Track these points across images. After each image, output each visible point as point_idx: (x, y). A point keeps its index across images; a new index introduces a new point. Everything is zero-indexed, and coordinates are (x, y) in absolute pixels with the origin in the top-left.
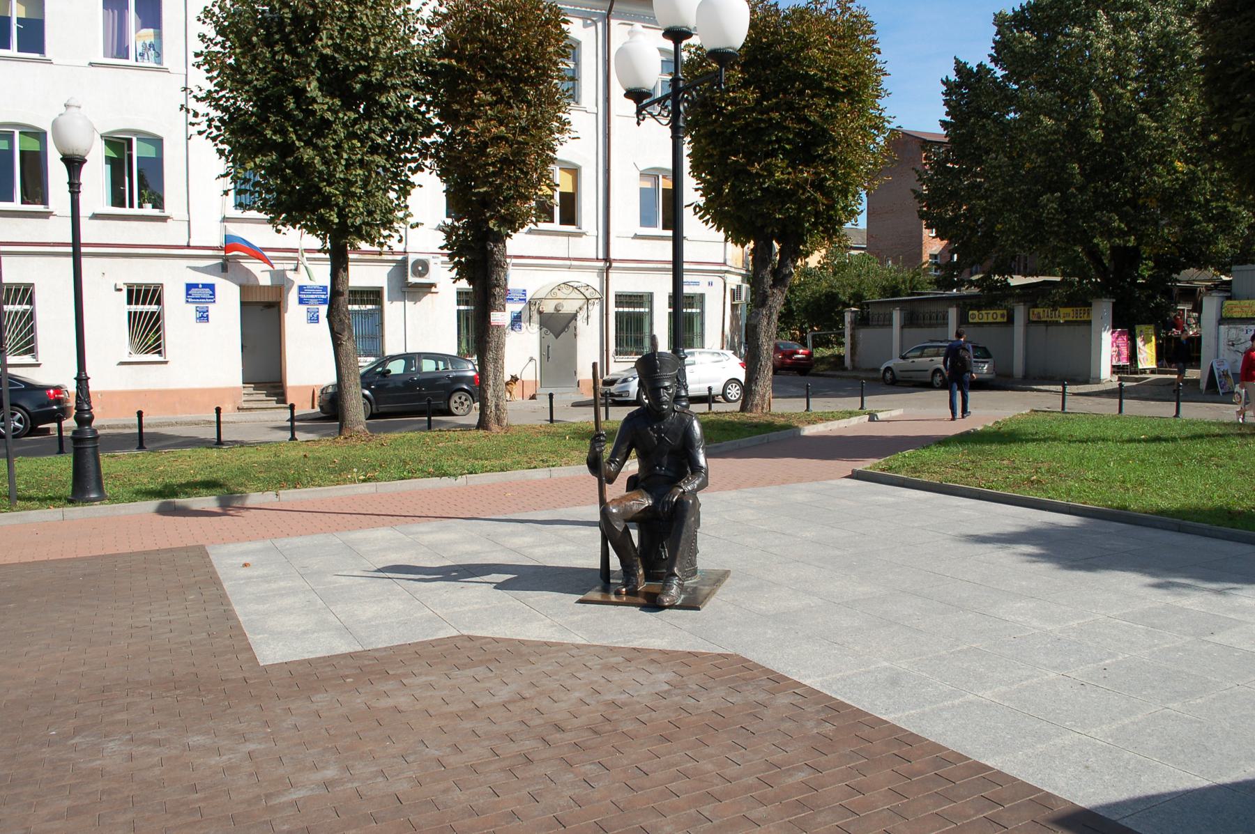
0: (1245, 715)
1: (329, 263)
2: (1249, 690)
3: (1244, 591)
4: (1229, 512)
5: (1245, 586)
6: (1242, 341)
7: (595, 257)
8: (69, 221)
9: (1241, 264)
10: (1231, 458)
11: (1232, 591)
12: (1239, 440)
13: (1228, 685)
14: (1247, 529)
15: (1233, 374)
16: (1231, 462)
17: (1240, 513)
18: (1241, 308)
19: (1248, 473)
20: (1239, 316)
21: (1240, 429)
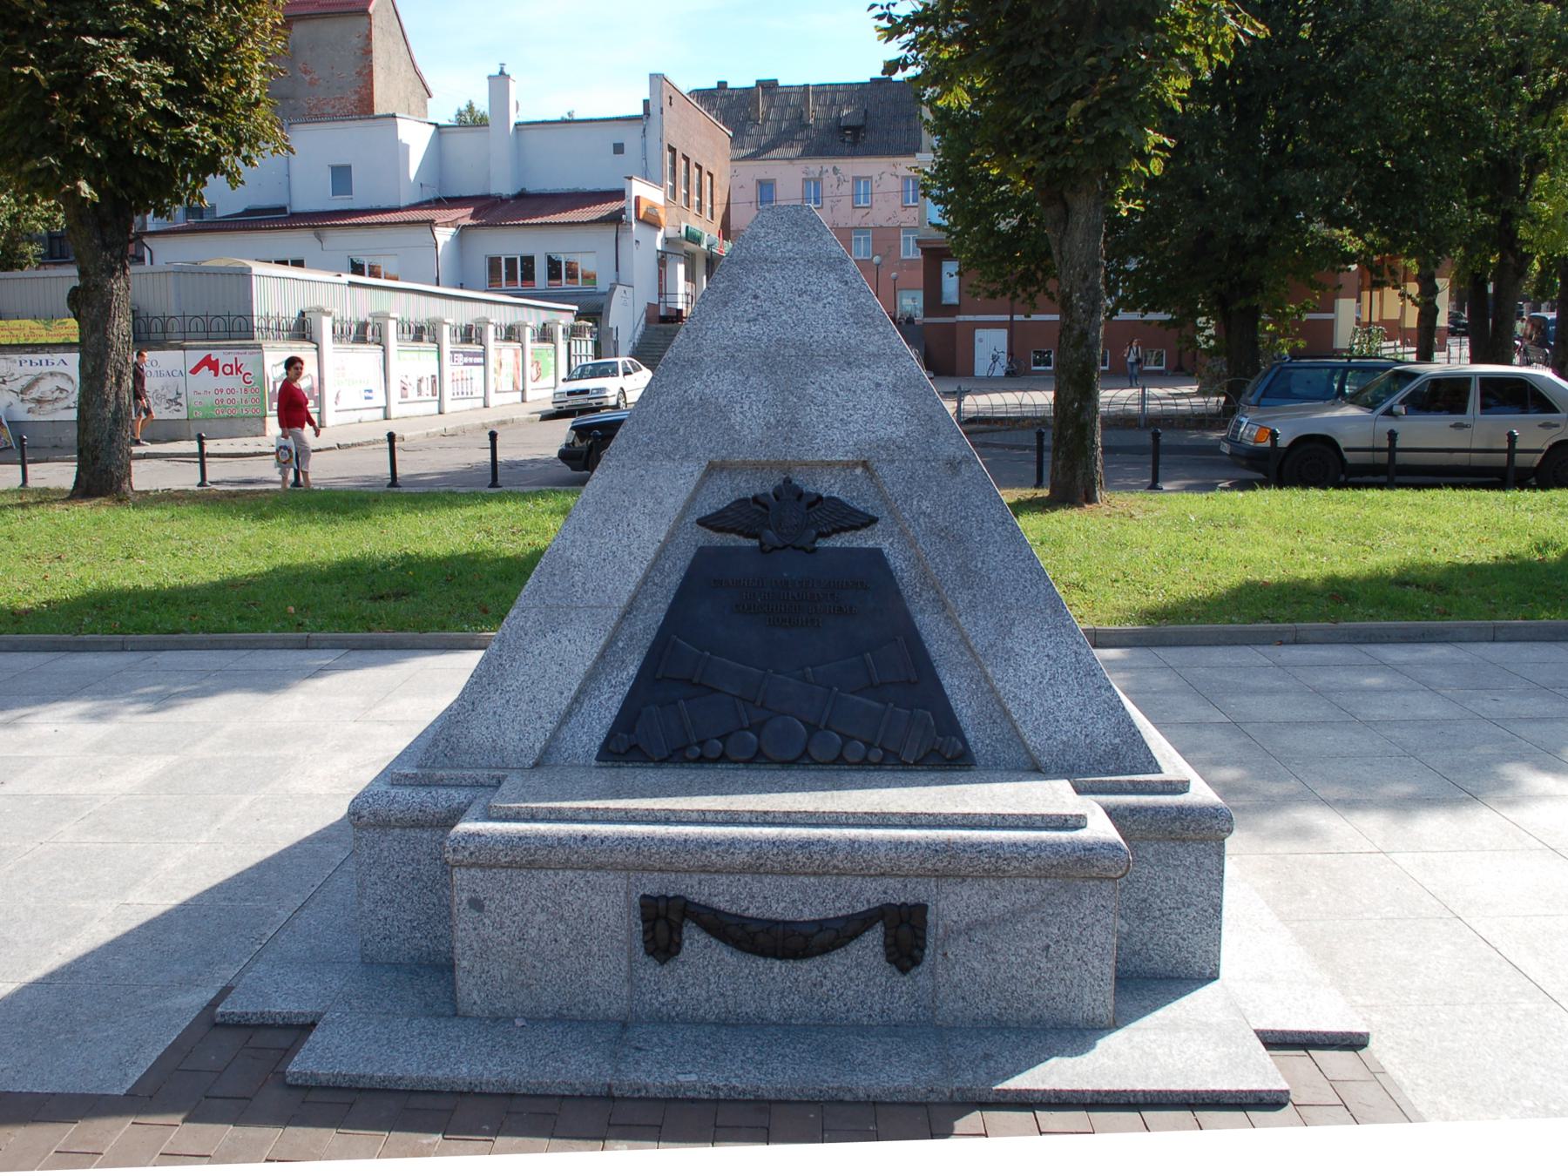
0: (53, 881)
1: (76, 464)
2: (55, 845)
3: (40, 717)
4: (13, 614)
5: (39, 708)
6: (16, 377)
7: (482, 367)
8: (388, 453)
9: (6, 270)
10: (11, 538)
11: (25, 720)
12: (19, 512)
13: (29, 847)
14: (37, 632)
15: (8, 422)
16: (11, 544)
17: (27, 612)
18: (10, 330)
19: (36, 556)
20: (8, 343)
21: (21, 498)
